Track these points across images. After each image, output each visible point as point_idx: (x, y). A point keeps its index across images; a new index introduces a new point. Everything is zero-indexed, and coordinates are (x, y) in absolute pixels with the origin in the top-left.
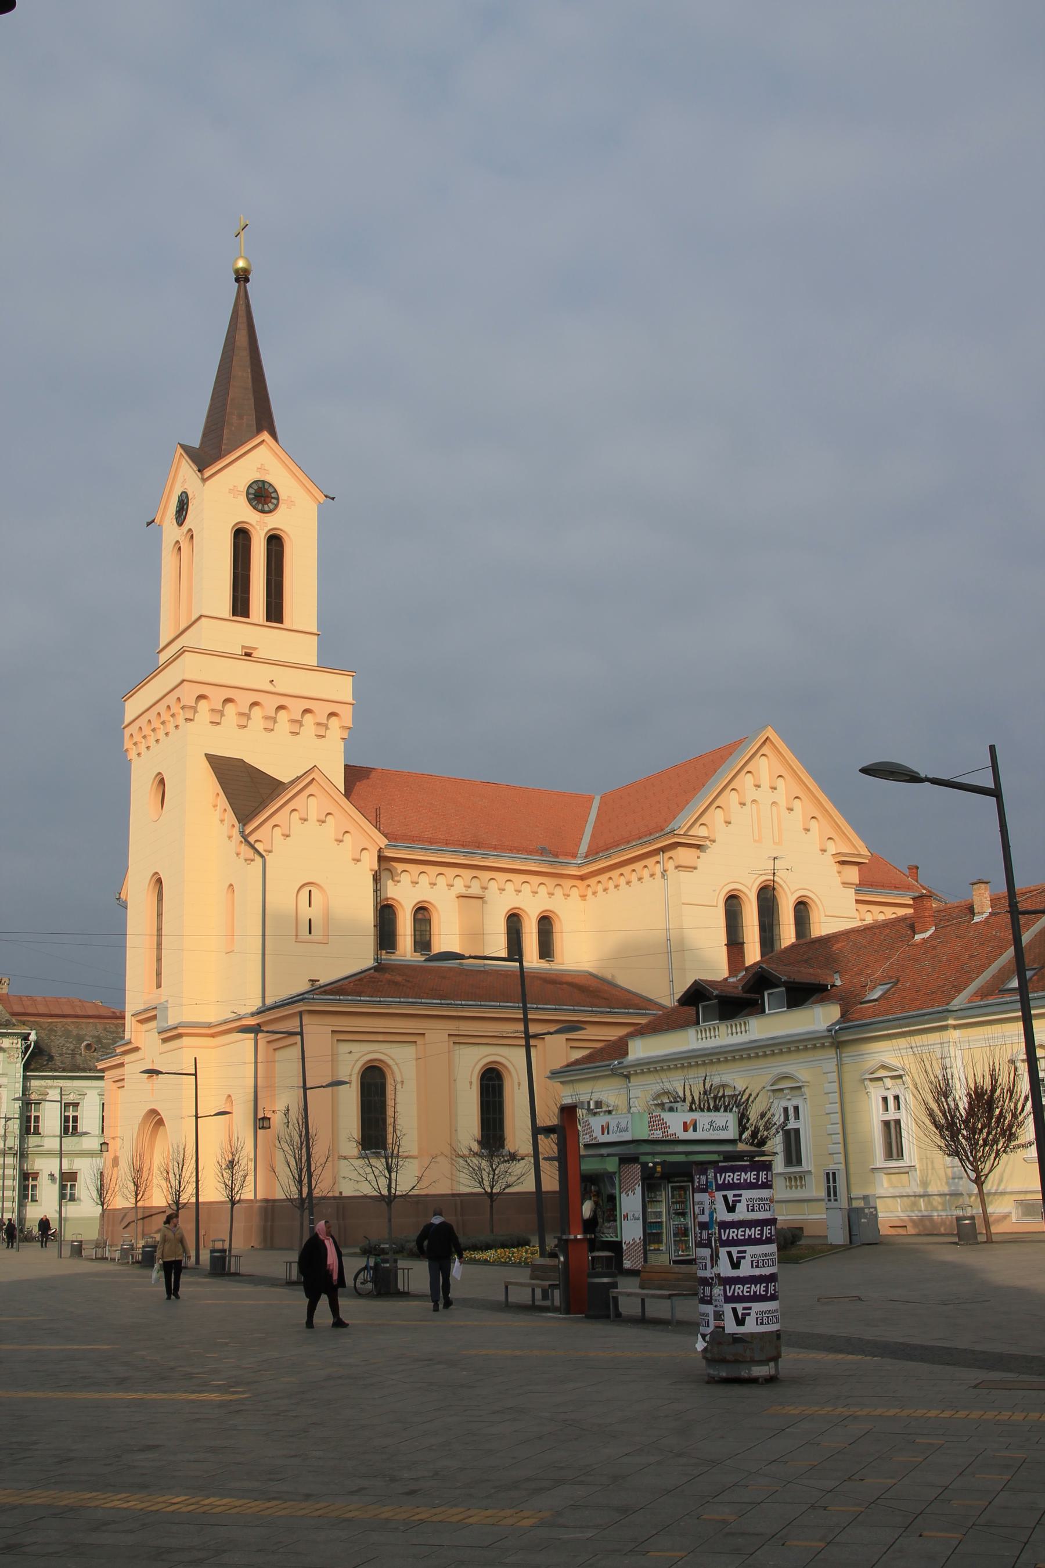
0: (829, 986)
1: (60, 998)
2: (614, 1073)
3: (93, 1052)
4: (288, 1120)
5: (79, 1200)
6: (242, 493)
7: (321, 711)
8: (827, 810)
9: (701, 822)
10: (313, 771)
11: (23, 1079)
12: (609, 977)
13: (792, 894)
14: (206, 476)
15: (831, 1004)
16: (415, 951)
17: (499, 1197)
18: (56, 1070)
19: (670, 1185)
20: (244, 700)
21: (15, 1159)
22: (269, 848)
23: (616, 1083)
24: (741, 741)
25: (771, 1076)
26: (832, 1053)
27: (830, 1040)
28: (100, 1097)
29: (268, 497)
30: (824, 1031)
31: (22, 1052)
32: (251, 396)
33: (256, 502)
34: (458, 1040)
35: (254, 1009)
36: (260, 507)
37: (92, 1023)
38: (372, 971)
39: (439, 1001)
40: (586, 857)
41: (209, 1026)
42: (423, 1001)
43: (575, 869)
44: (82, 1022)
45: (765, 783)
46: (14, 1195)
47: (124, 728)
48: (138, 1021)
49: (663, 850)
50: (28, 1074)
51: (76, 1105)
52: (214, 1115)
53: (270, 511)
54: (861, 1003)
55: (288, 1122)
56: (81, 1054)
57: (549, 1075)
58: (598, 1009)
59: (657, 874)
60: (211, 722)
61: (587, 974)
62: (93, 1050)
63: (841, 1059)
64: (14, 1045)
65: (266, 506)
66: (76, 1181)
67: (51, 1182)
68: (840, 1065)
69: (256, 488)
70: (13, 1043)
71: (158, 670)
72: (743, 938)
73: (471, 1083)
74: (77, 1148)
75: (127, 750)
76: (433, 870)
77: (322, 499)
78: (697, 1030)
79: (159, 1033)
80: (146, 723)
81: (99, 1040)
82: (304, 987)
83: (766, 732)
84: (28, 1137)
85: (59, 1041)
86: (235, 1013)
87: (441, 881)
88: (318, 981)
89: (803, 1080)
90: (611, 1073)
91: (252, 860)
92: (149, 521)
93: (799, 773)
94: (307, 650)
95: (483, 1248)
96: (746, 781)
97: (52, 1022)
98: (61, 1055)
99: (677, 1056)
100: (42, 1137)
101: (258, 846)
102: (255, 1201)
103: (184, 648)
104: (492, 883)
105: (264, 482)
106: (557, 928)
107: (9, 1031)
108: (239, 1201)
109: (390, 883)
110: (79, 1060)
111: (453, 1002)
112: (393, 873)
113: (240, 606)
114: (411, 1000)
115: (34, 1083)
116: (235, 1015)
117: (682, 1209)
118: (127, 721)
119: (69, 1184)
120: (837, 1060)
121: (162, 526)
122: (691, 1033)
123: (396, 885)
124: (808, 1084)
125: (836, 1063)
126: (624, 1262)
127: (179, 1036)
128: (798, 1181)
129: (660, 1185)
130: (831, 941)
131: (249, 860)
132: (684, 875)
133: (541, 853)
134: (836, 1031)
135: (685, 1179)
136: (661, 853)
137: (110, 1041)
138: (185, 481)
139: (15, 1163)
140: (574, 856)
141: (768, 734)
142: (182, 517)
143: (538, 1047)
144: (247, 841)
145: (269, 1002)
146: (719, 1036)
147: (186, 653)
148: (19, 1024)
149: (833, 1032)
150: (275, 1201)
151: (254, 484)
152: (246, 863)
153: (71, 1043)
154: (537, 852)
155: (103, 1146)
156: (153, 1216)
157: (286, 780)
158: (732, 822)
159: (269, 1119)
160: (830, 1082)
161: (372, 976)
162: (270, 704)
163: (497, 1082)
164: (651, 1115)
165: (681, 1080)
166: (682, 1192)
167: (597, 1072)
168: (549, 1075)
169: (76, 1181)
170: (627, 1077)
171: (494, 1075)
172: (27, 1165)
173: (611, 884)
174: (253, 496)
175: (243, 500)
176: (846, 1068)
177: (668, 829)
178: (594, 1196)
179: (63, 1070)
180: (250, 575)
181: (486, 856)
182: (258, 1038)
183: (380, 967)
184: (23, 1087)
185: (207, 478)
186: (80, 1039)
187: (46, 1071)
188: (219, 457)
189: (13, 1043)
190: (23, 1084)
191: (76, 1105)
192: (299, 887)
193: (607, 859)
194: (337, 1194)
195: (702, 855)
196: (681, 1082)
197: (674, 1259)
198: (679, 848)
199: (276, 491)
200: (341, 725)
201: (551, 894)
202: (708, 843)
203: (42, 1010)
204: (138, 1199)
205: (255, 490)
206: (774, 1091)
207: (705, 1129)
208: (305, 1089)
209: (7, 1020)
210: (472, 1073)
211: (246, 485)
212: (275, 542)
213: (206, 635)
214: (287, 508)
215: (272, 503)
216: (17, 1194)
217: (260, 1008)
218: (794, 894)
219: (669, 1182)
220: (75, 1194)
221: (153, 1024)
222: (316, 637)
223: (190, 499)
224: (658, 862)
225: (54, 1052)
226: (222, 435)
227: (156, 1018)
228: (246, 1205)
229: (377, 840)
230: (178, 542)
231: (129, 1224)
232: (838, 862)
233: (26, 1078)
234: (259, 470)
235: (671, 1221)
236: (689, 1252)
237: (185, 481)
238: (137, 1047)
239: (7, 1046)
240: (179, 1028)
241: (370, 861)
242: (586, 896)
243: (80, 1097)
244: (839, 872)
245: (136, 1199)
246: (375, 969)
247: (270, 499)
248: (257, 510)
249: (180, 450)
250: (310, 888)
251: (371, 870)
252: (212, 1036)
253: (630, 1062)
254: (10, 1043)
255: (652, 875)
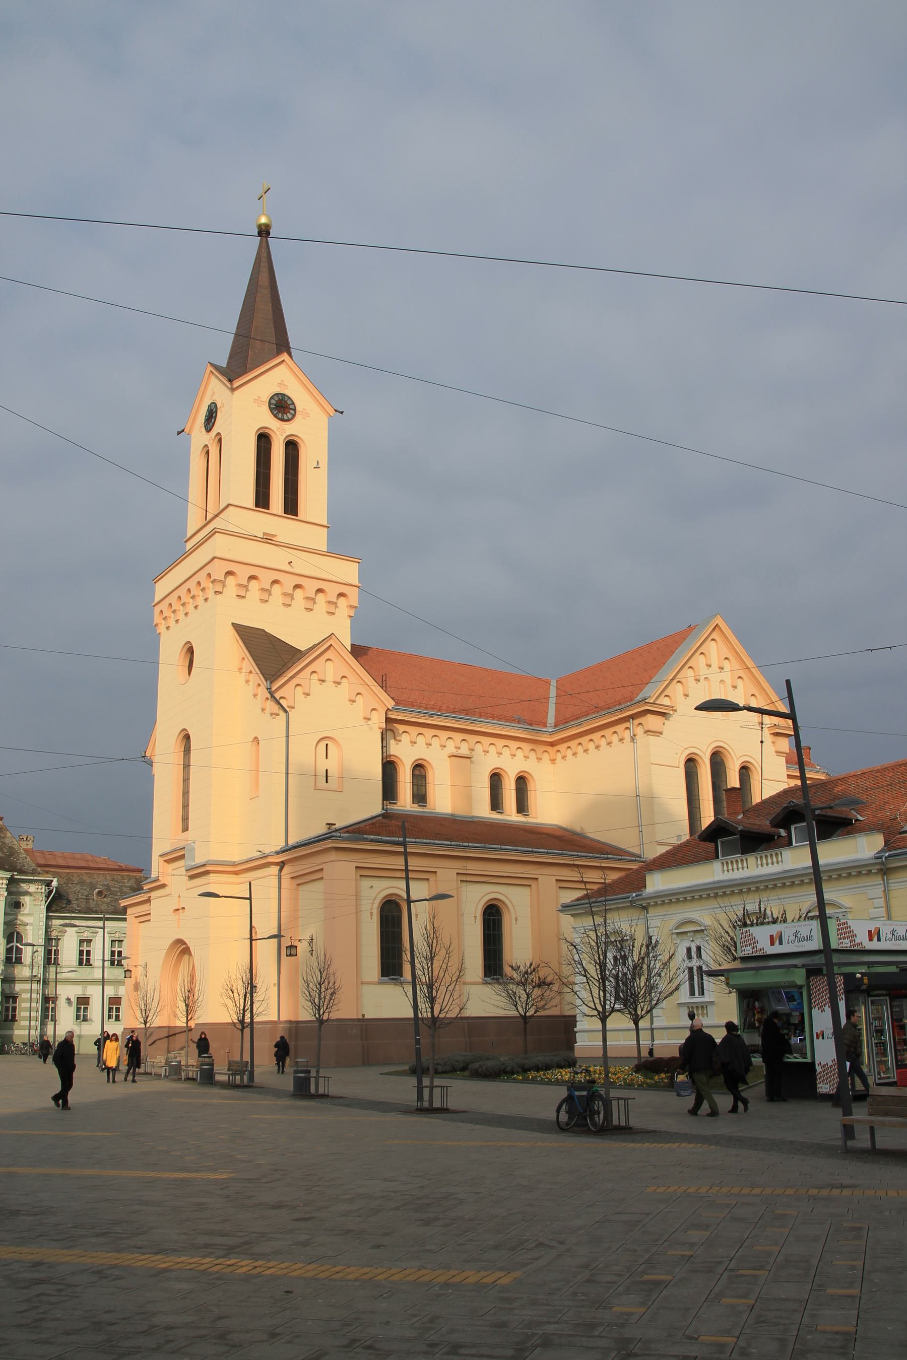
0: (853, 820)
1: (75, 854)
2: (632, 905)
3: (104, 898)
4: (312, 949)
5: (91, 1020)
6: (264, 403)
7: (332, 591)
8: (764, 689)
9: (665, 693)
10: (331, 639)
11: (46, 918)
12: (578, 830)
13: (737, 759)
14: (235, 386)
15: (876, 833)
16: (413, 803)
17: (531, 1020)
18: (73, 912)
19: (870, 999)
20: (266, 577)
21: (39, 985)
22: (292, 705)
23: (634, 914)
24: (691, 628)
25: (675, 921)
26: (878, 880)
27: (878, 867)
28: (110, 935)
29: (286, 408)
30: (870, 859)
31: (46, 896)
32: (272, 325)
33: (277, 411)
34: (465, 878)
35: (278, 848)
36: (280, 415)
37: (102, 874)
38: (381, 818)
39: (449, 843)
40: (556, 726)
41: (234, 864)
42: (436, 842)
43: (547, 736)
44: (94, 873)
45: (715, 665)
46: (38, 1015)
47: (154, 606)
48: (165, 861)
49: (633, 717)
50: (50, 914)
51: (89, 941)
52: (268, 938)
53: (288, 420)
54: (901, 833)
55: (312, 950)
56: (93, 899)
57: (560, 908)
58: (583, 854)
59: (626, 739)
60: (237, 596)
61: (556, 827)
62: (103, 896)
63: (888, 887)
64: (39, 890)
65: (285, 415)
66: (88, 1005)
67: (68, 1005)
68: (886, 892)
69: (277, 399)
70: (38, 889)
71: (187, 554)
72: (699, 796)
73: (475, 917)
74: (89, 977)
75: (156, 625)
76: (429, 732)
77: (332, 412)
78: (757, 858)
79: (186, 871)
80: (176, 599)
81: (108, 888)
82: (322, 830)
83: (716, 620)
84: (49, 967)
85: (75, 889)
86: (260, 852)
87: (436, 742)
88: (335, 824)
89: (847, 906)
90: (630, 904)
91: (277, 715)
92: (180, 431)
93: (742, 656)
94: (319, 539)
95: (544, 1068)
96: (699, 661)
97: (69, 873)
98: (77, 899)
99: (712, 886)
100: (61, 967)
101: (282, 702)
102: (279, 1022)
103: (216, 530)
104: (479, 746)
105: (284, 395)
106: (531, 786)
107: (35, 878)
108: (326, 1021)
109: (392, 742)
110: (92, 904)
111: (461, 844)
112: (396, 733)
113: (262, 500)
114: (425, 841)
115: (56, 922)
116: (260, 853)
117: (880, 1026)
118: (157, 599)
119: (82, 1007)
120: (885, 886)
121: (191, 435)
122: (716, 866)
123: (397, 744)
124: (850, 910)
125: (883, 889)
126: (819, 1086)
127: (207, 873)
128: (700, 1010)
129: (858, 999)
130: (827, 786)
131: (275, 714)
132: (652, 739)
133: (518, 722)
134: (886, 858)
135: (884, 992)
136: (631, 720)
137: (118, 889)
138: (214, 394)
139: (39, 988)
140: (545, 726)
141: (717, 622)
142: (211, 424)
143: (532, 886)
144: (272, 696)
145: (292, 842)
146: (782, 861)
147: (217, 534)
148: (44, 873)
149: (884, 859)
150: (298, 1022)
151: (275, 396)
152: (271, 718)
153: (85, 890)
154: (514, 720)
155: (127, 973)
156: (176, 1035)
157: (303, 648)
158: (690, 695)
159: (296, 947)
160: (875, 908)
161: (381, 821)
162: (289, 582)
163: (496, 918)
164: (839, 922)
165: (740, 904)
166: (880, 1007)
167: (619, 903)
168: (560, 908)
169: (88, 1005)
170: (645, 908)
171: (494, 911)
172: (48, 990)
173: (569, 752)
174: (275, 406)
175: (265, 409)
176: (892, 894)
177: (639, 698)
178: (758, 1013)
179: (79, 912)
180: (270, 473)
181: (473, 722)
182: (282, 874)
183: (386, 816)
184: (46, 925)
185: (235, 388)
186: (92, 887)
187: (65, 913)
188: (245, 372)
189: (38, 889)
190: (46, 923)
191: (89, 941)
192: (317, 741)
193: (578, 727)
194: (361, 1017)
195: (666, 722)
196: (739, 906)
197: (878, 1081)
198: (648, 715)
199: (293, 403)
200: (348, 605)
201: (526, 757)
202: (671, 712)
203: (61, 862)
204: (189, 1019)
205: (276, 401)
206: (678, 934)
207: (887, 938)
208: (251, 940)
209: (33, 869)
210: (476, 907)
211: (268, 397)
212: (292, 447)
213: (235, 520)
214: (303, 418)
215: (291, 413)
216: (40, 1015)
217: (284, 847)
218: (739, 759)
219: (869, 996)
220: (87, 1016)
221: (181, 863)
222: (326, 529)
223: (218, 408)
224: (627, 728)
225: (72, 897)
226: (247, 356)
227: (184, 857)
228: (270, 1026)
229: (385, 702)
230: (206, 446)
231: (155, 1041)
232: (773, 734)
233: (48, 918)
234: (279, 385)
235: (873, 1039)
236: (890, 1074)
237: (214, 394)
238: (164, 884)
239: (33, 891)
240: (207, 865)
241: (378, 720)
242: (555, 760)
243: (93, 934)
244: (773, 743)
245: (187, 1019)
246: (383, 815)
247: (288, 409)
248: (278, 419)
249: (210, 368)
250: (327, 742)
251: (380, 728)
252: (236, 873)
253: (649, 894)
254: (35, 888)
255: (621, 740)
